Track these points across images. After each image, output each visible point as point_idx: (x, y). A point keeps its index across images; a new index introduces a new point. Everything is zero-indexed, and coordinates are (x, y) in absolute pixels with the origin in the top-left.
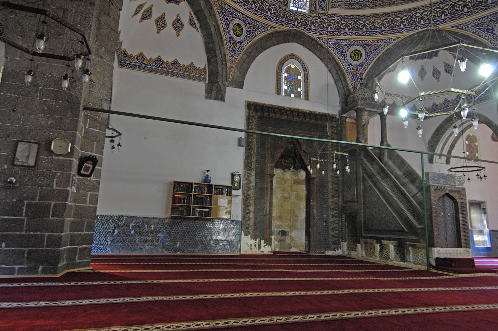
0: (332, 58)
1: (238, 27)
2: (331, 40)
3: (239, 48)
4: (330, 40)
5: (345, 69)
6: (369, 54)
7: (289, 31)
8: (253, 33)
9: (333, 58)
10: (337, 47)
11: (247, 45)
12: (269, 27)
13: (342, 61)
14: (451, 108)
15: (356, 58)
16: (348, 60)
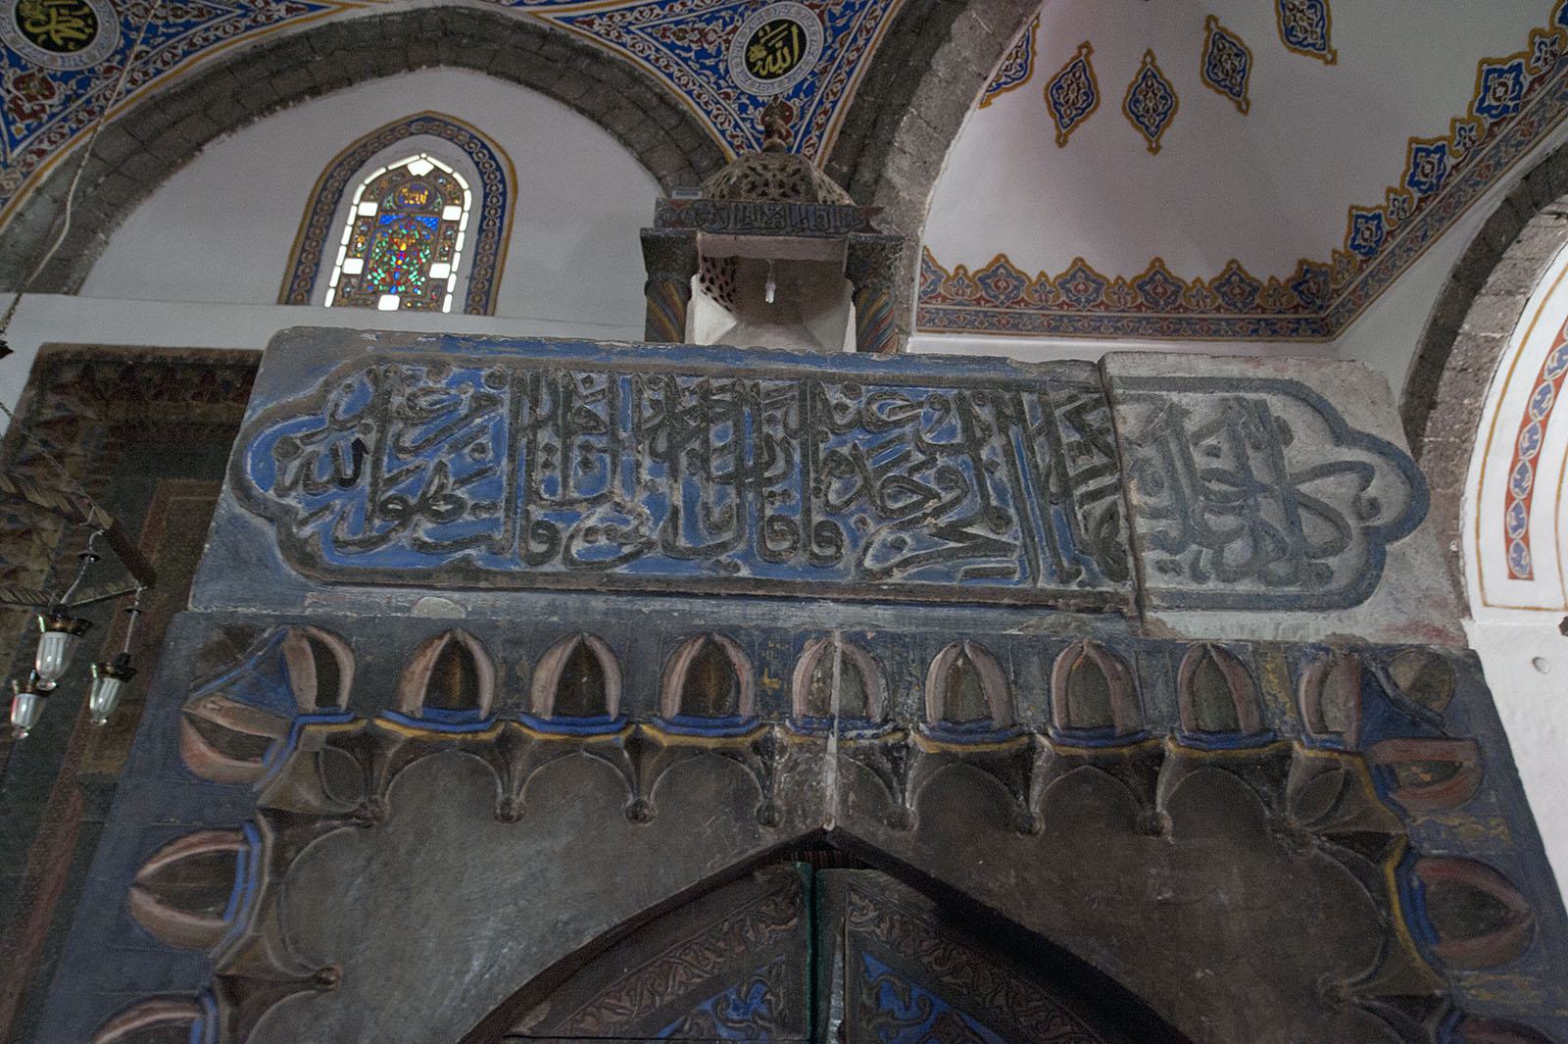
0: (655, 101)
2: (636, 13)
4: (630, 17)
5: (723, 132)
6: (840, 23)
9: (662, 99)
10: (670, 39)
11: (122, 96)
13: (705, 98)
14: (1465, 180)
15: (775, 62)
16: (736, 87)
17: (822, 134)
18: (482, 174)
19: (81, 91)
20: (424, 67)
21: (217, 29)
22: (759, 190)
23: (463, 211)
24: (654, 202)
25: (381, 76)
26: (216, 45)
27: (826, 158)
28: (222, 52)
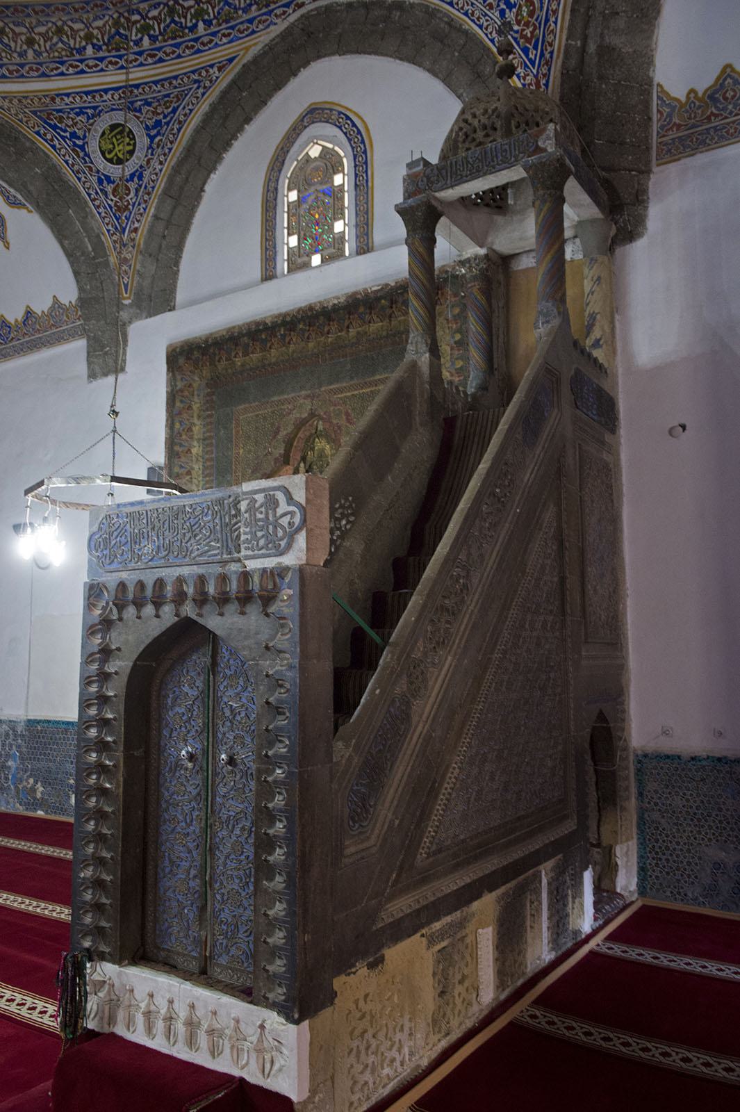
0: (447, 29)
1: (115, 136)
3: (136, 195)
7: (288, 32)
8: (167, 124)
12: (215, 69)
17: (557, 19)
18: (349, 140)
19: (141, 182)
20: (302, 69)
21: (188, 105)
22: (470, 139)
23: (344, 174)
24: (402, 180)
25: (280, 89)
26: (192, 114)
27: (564, 37)
28: (195, 119)
